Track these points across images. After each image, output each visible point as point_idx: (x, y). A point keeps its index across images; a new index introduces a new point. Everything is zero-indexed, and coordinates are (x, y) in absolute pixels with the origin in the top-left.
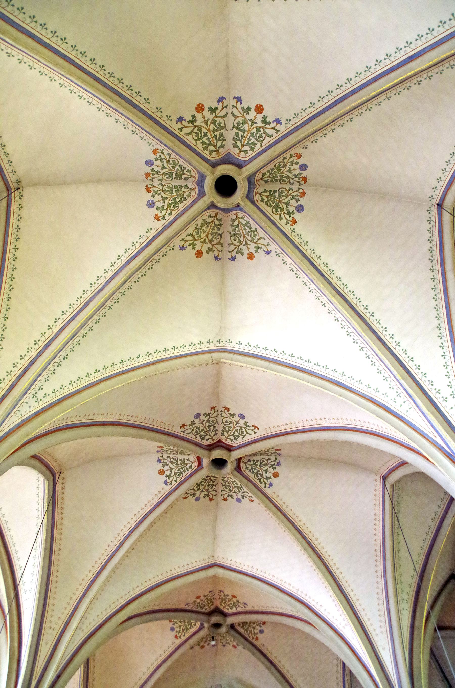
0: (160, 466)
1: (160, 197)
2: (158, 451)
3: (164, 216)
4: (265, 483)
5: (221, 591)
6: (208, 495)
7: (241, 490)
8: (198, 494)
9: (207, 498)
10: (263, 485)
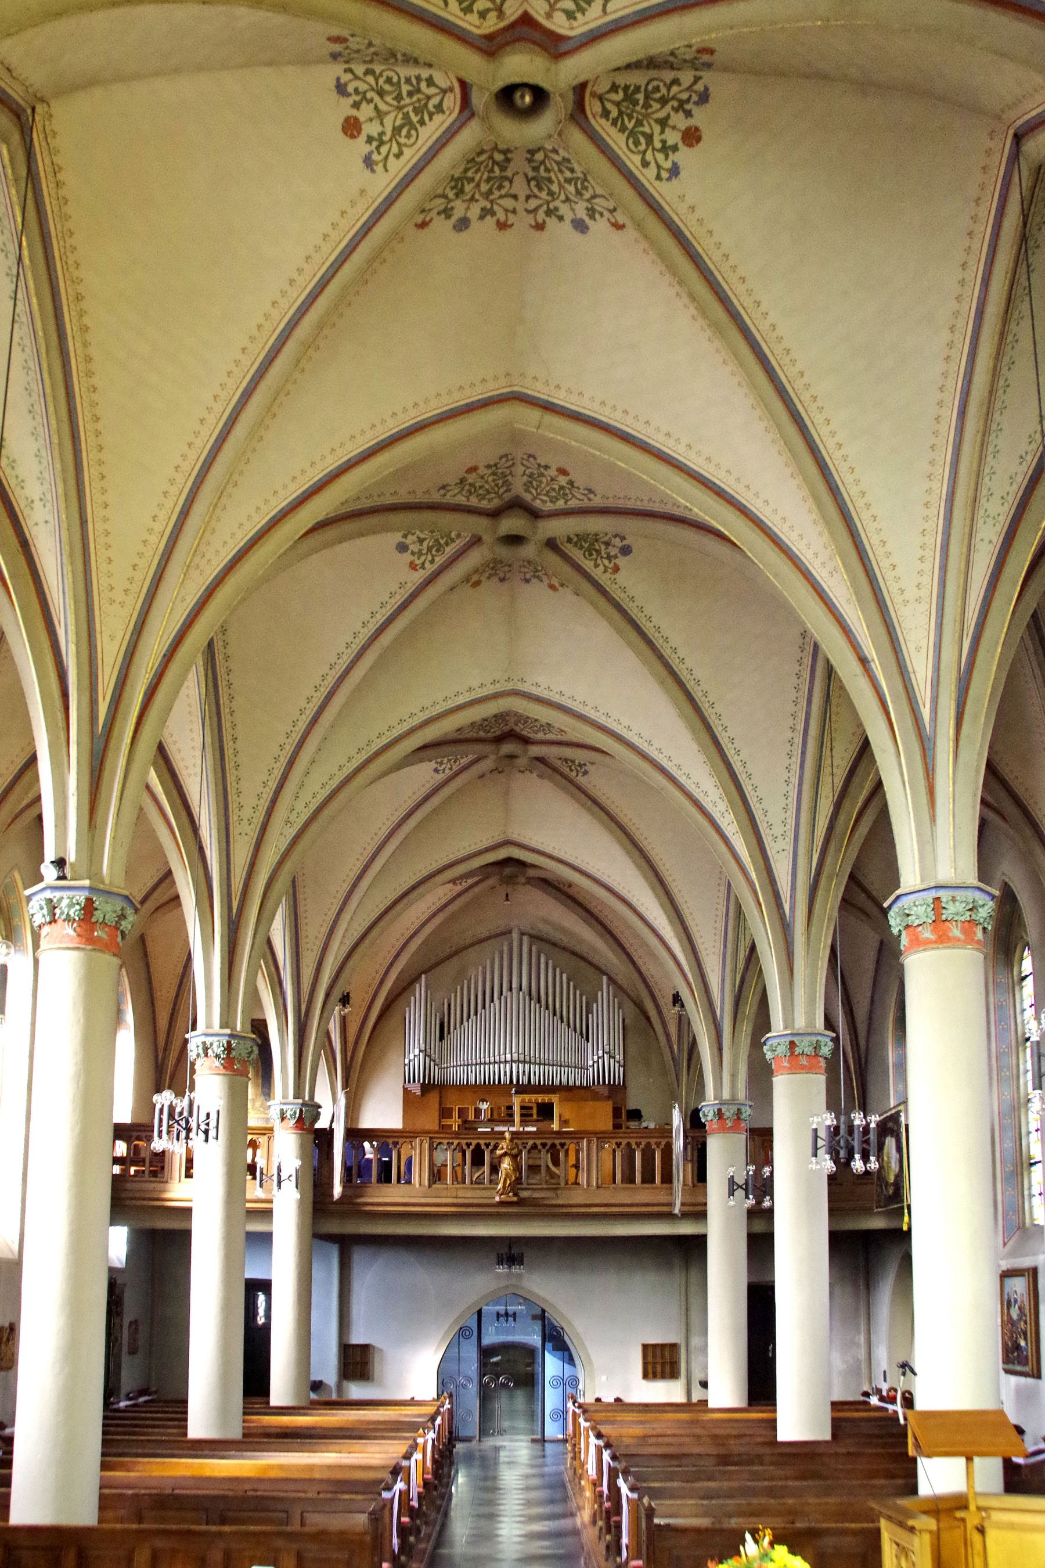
0: (344, 108)
1: (414, 538)
2: (335, 56)
3: (423, 564)
4: (659, 167)
5: (530, 456)
6: (493, 213)
7: (586, 188)
8: (459, 209)
9: (490, 220)
10: (574, 774)
